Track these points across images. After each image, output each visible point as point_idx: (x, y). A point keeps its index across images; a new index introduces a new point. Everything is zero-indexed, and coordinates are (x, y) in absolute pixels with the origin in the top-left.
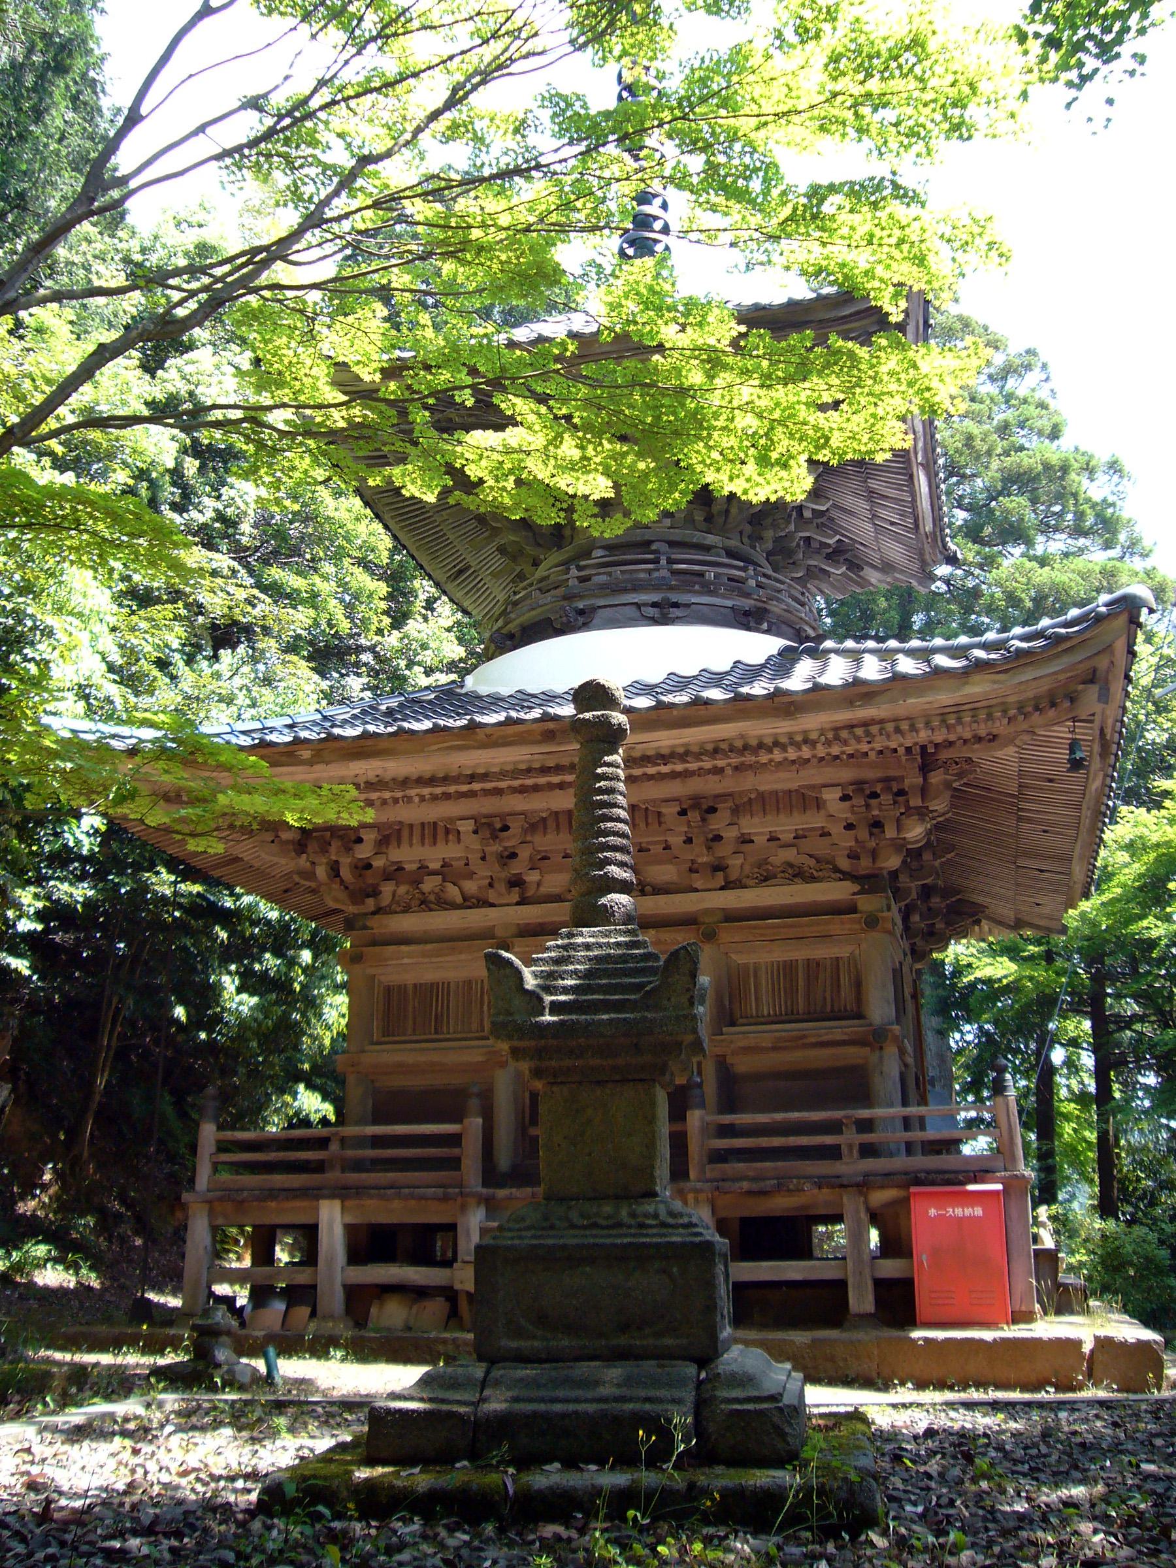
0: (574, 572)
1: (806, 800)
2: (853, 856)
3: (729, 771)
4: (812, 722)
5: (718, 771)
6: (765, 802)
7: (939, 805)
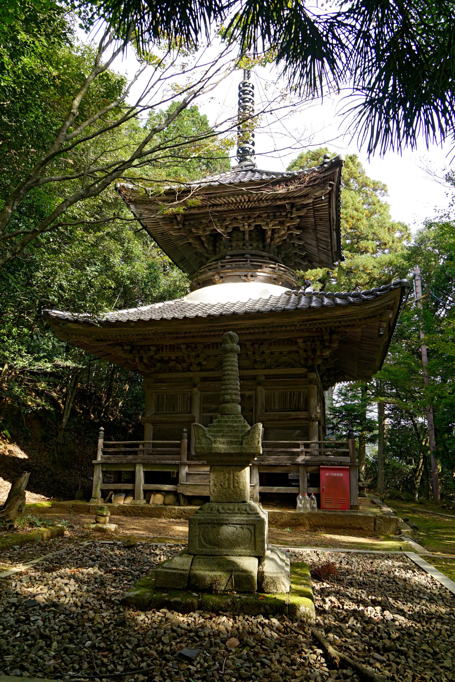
0: (220, 264)
1: (292, 342)
2: (306, 359)
3: (268, 333)
4: (296, 319)
5: (264, 333)
6: (278, 342)
7: (335, 345)
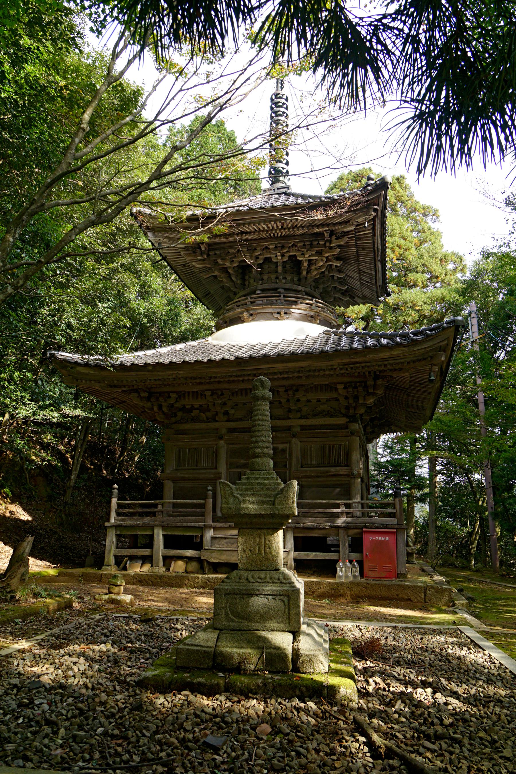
0: (249, 300)
1: (331, 388)
2: (347, 408)
3: (304, 378)
4: (335, 362)
5: (299, 378)
6: (316, 388)
7: (380, 392)
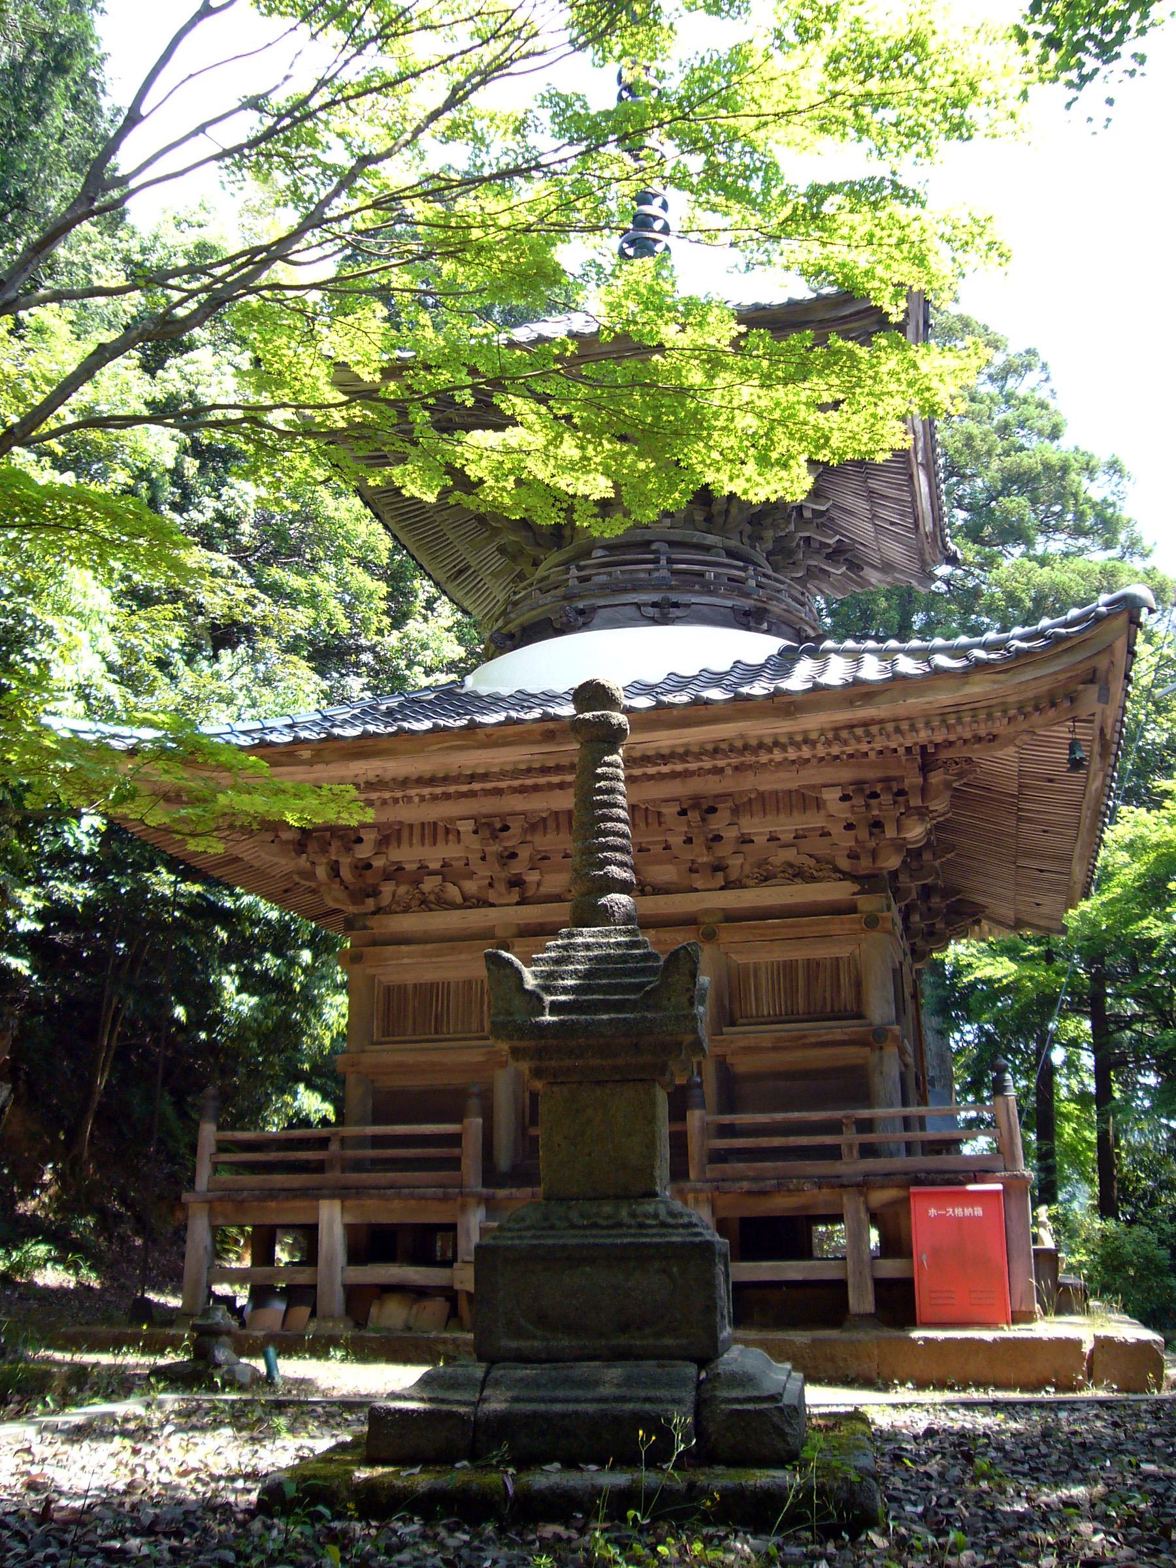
0: (574, 572)
1: (806, 800)
2: (853, 856)
3: (729, 771)
4: (812, 722)
5: (718, 771)
6: (765, 802)
7: (939, 805)
